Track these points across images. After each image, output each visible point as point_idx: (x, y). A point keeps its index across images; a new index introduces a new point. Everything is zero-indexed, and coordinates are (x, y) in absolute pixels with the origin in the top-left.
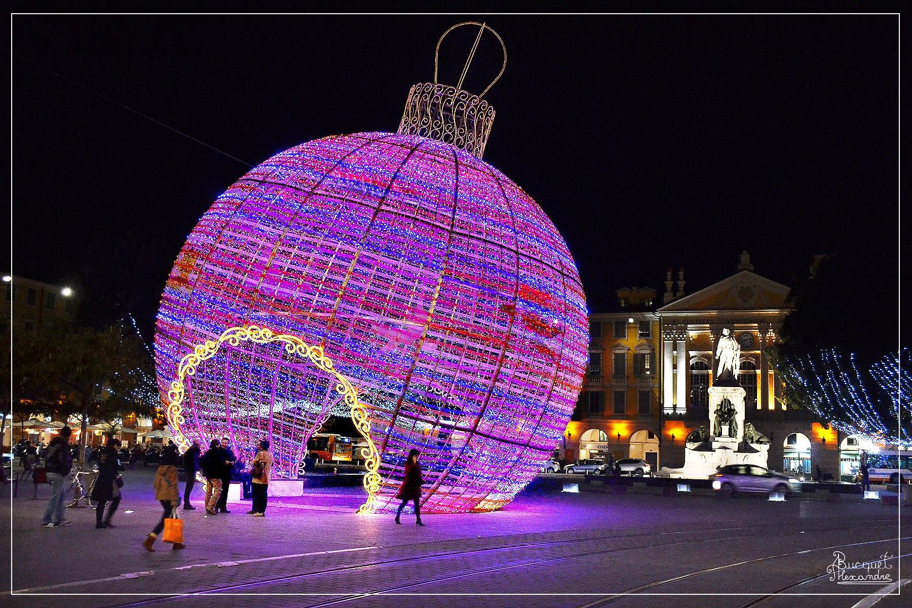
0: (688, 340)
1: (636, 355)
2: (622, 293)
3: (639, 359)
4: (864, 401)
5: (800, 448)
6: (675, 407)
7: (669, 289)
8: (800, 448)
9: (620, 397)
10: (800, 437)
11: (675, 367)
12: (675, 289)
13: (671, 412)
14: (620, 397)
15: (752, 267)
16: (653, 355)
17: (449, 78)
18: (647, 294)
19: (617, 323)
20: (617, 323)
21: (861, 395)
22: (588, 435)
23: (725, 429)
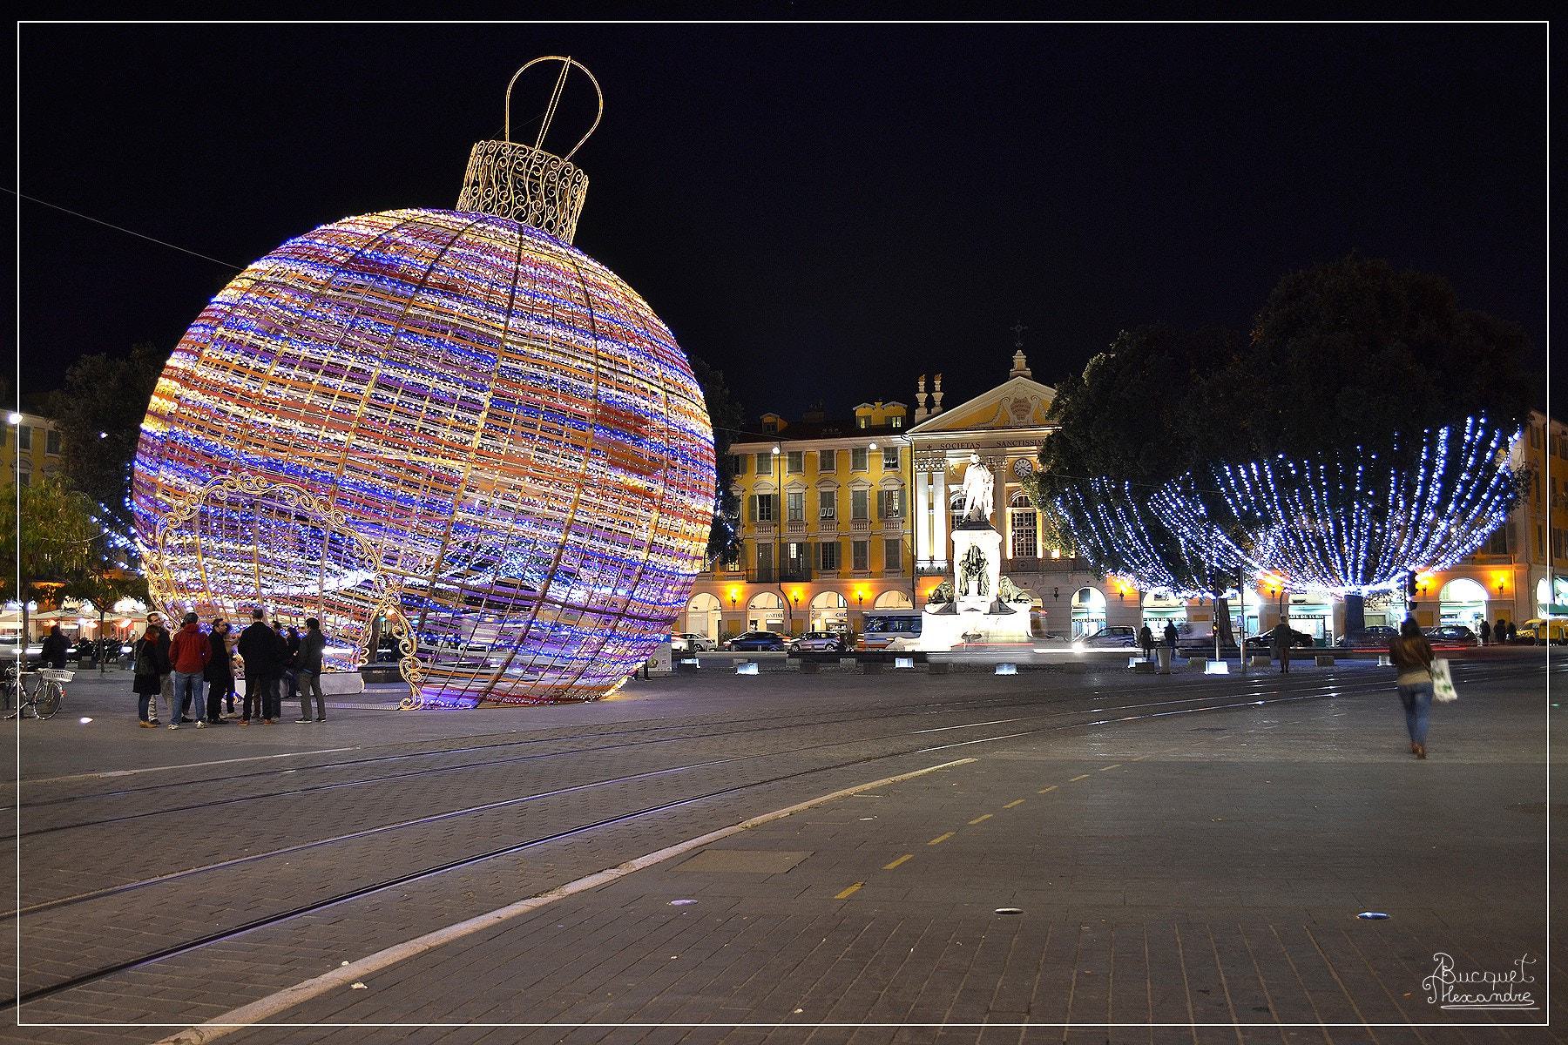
0: (947, 471)
1: (880, 493)
2: (862, 411)
3: (885, 498)
4: (1144, 543)
5: (1093, 609)
6: (932, 560)
7: (922, 404)
8: (1093, 609)
9: (860, 548)
10: (1094, 593)
11: (931, 507)
12: (930, 403)
13: (926, 565)
14: (860, 548)
15: (1028, 372)
16: (902, 492)
17: (524, 135)
18: (893, 411)
19: (760, 456)
20: (760, 456)
21: (1140, 536)
22: (821, 600)
23: (973, 585)
